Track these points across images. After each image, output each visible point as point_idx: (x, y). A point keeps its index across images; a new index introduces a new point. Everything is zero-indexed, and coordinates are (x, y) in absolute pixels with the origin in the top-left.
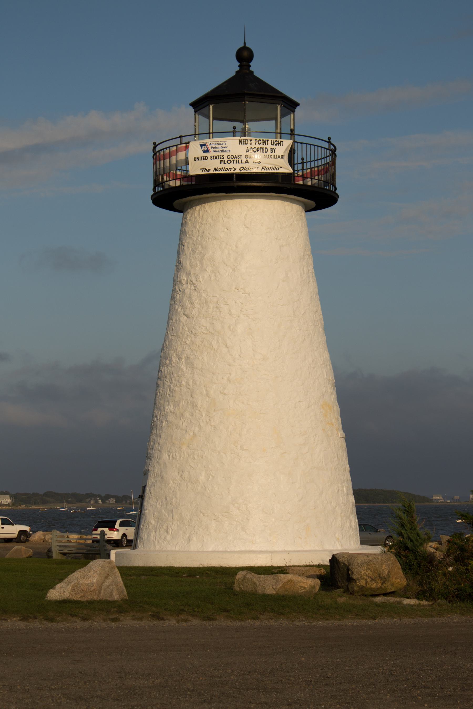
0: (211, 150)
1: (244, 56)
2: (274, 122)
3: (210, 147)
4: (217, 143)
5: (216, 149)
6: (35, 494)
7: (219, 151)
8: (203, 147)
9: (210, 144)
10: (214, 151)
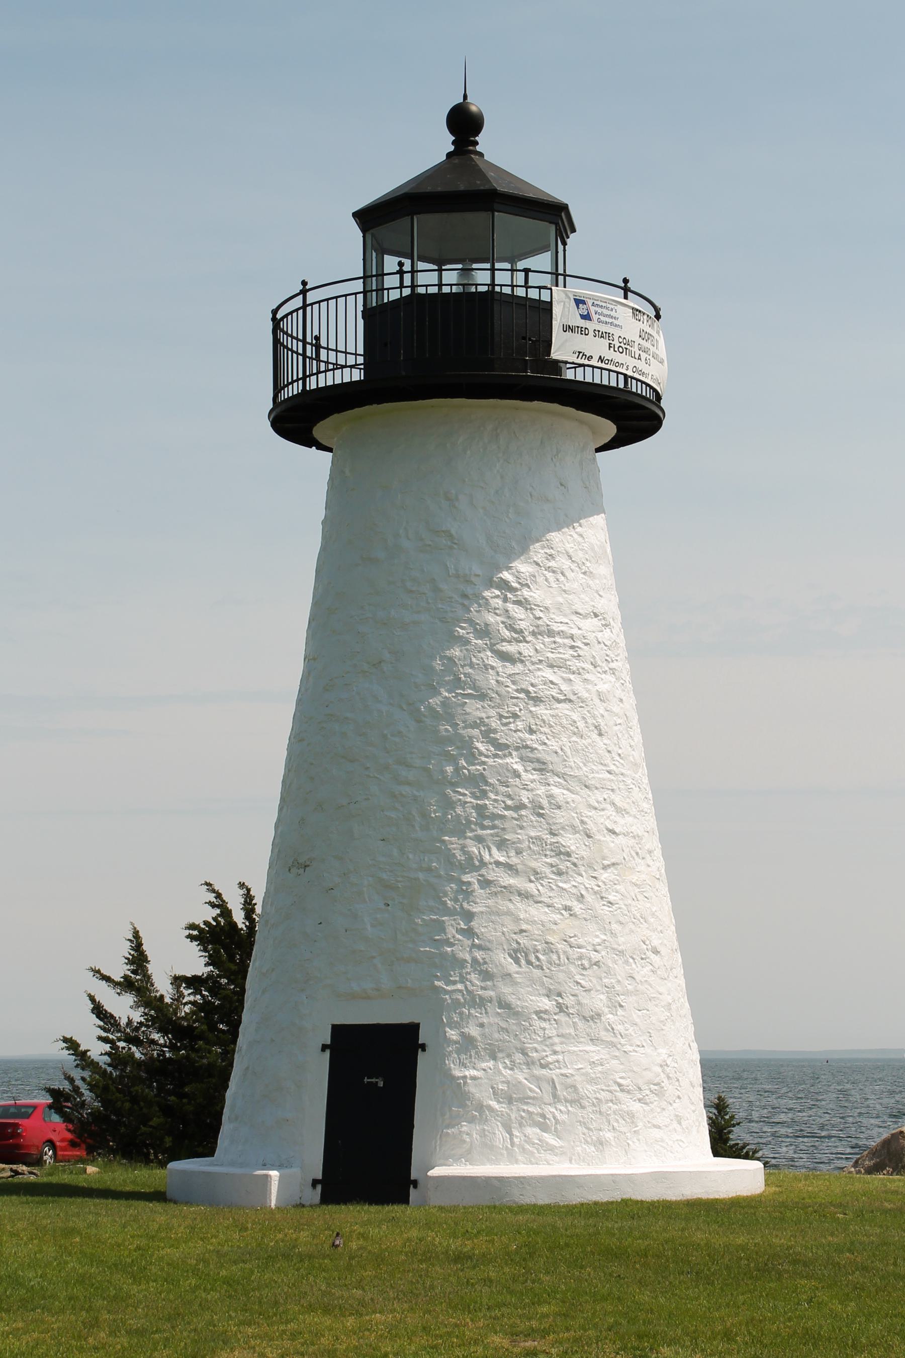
0: (595, 317)
1: (464, 123)
2: (530, 273)
3: (593, 309)
4: (604, 304)
5: (602, 318)
6: (112, 1016)
7: (606, 323)
8: (581, 305)
9: (593, 304)
10: (599, 321)
